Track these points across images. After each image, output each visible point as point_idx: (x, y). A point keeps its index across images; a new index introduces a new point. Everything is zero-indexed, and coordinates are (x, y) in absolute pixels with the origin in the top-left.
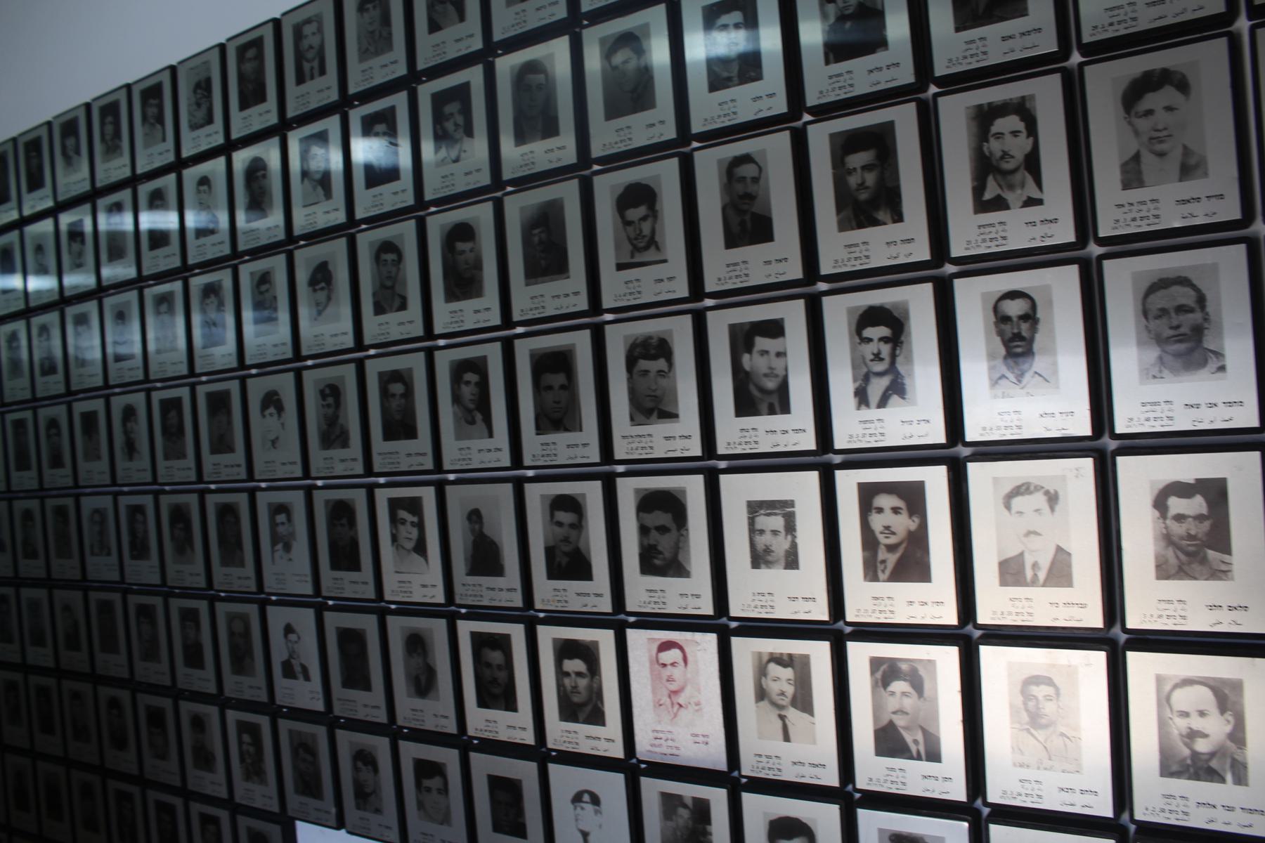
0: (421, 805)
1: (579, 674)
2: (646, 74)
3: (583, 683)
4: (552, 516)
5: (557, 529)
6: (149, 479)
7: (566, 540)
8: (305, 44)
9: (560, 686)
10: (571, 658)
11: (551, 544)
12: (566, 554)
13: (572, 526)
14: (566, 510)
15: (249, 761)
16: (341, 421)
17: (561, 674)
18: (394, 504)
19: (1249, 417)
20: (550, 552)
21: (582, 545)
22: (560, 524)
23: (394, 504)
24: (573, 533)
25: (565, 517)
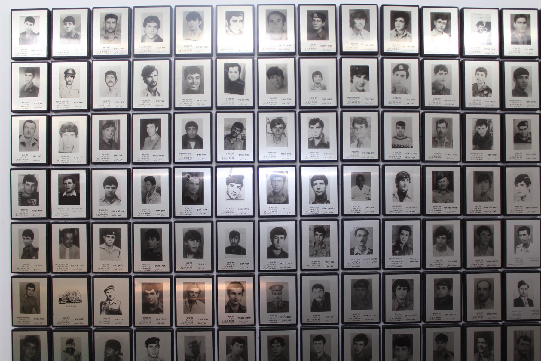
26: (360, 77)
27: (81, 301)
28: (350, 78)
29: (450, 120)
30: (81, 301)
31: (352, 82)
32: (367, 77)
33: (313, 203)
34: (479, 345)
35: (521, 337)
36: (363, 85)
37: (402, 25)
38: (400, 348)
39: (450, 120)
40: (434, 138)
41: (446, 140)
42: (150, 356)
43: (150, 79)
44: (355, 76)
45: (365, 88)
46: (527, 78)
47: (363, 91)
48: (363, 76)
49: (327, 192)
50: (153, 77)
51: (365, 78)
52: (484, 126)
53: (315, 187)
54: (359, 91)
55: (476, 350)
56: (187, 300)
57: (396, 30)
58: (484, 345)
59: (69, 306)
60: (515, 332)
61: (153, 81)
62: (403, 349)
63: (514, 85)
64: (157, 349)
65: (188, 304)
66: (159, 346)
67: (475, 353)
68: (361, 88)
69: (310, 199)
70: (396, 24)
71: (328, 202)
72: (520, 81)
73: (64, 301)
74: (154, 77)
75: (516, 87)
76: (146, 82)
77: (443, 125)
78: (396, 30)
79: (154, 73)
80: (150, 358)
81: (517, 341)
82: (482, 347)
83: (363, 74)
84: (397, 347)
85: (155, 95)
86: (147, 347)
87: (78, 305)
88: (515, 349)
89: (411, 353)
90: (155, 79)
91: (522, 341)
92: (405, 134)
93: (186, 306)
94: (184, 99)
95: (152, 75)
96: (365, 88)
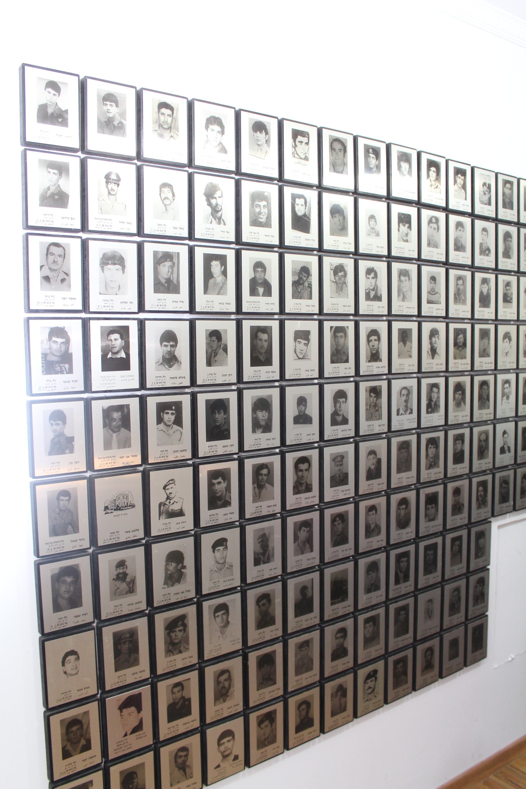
27: (133, 506)
30: (133, 506)
33: (369, 361)
53: (371, 344)
56: (256, 485)
59: (118, 516)
65: (257, 490)
69: (367, 358)
71: (381, 361)
73: (112, 509)
87: (130, 511)
94: (251, 233)
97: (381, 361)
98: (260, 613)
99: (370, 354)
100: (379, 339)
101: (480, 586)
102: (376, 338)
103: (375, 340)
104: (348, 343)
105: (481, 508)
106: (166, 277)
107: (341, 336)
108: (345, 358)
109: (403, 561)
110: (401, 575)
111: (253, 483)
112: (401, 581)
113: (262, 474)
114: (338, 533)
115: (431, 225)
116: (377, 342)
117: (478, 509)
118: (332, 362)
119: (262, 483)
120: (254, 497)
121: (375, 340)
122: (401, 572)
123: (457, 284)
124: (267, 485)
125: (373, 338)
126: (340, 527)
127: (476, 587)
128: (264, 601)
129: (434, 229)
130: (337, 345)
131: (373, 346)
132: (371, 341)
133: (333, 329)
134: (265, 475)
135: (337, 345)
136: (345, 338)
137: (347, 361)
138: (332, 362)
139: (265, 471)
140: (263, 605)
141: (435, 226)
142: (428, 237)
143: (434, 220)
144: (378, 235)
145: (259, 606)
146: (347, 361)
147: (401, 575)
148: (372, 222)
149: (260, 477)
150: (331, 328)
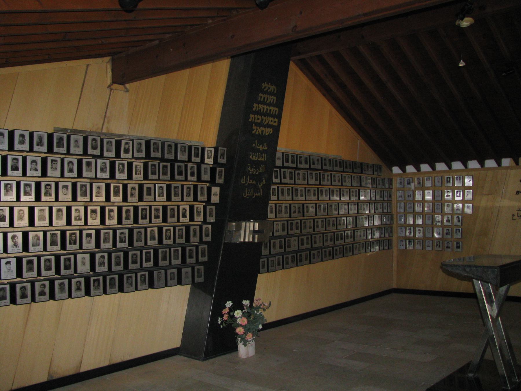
0: (308, 195)
1: (154, 168)
2: (411, 207)
3: (154, 170)
4: (13, 161)
5: (14, 163)
6: (293, 183)
7: (15, 165)
8: (137, 169)
9: (151, 170)
10: (153, 166)
11: (12, 165)
12: (15, 167)
13: (16, 162)
14: (15, 160)
15: (120, 170)
16: (141, 148)
17: (151, 168)
18: (310, 173)
19: (209, 180)
20: (12, 167)
21: (18, 165)
22: (14, 162)
23: (310, 173)
24: (16, 164)
25: (15, 161)
26: (89, 238)
28: (85, 238)
29: (109, 232)
31: (86, 240)
32: (91, 238)
33: (69, 172)
34: (120, 167)
35: (117, 257)
36: (90, 241)
37: (97, 284)
38: (93, 214)
39: (109, 232)
40: (104, 240)
41: (108, 241)
42: (7, 269)
43: (15, 240)
44: (87, 238)
45: (90, 242)
46: (130, 213)
47: (90, 243)
48: (90, 237)
49: (73, 168)
50: (16, 239)
51: (90, 238)
52: (127, 145)
53: (69, 166)
54: (89, 243)
55: (119, 170)
56: (5, 190)
57: (95, 287)
58: (122, 168)
60: (115, 255)
61: (16, 241)
62: (94, 214)
63: (126, 215)
64: (10, 266)
65: (6, 192)
66: (11, 264)
67: (119, 171)
68: (89, 242)
69: (67, 171)
70: (95, 284)
71: (74, 172)
72: (127, 214)
74: (16, 240)
75: (126, 216)
76: (13, 241)
77: (107, 235)
78: (95, 287)
79: (16, 238)
80: (8, 270)
81: (116, 258)
82: (121, 169)
83: (90, 236)
84: (92, 214)
85: (17, 247)
86: (6, 265)
88: (115, 261)
89: (97, 216)
90: (17, 240)
91: (117, 258)
92: (100, 192)
93: (5, 193)
95: (15, 239)
96: (90, 242)
97: (74, 172)
98: (22, 293)
99: (69, 169)
100: (73, 165)
101: (102, 259)
102: (72, 164)
103: (71, 165)
104: (57, 239)
105: (121, 174)
106: (2, 295)
107: (55, 237)
108: (56, 244)
109: (73, 236)
110: (72, 242)
111: (4, 189)
112: (73, 244)
113: (8, 187)
114: (47, 266)
115: (108, 144)
116: (72, 166)
117: (120, 174)
118: (51, 245)
119: (8, 190)
120: (5, 194)
121: (71, 165)
122: (72, 240)
123: (105, 236)
124: (10, 191)
125: (70, 164)
126: (48, 264)
127: (100, 259)
128: (24, 289)
129: (110, 145)
130: (53, 240)
131: (70, 167)
132: (70, 165)
133: (51, 234)
134: (9, 187)
135: (53, 240)
136: (56, 237)
137: (57, 245)
138: (51, 245)
139: (9, 186)
140: (23, 290)
141: (110, 144)
142: (107, 148)
143: (109, 142)
144: (79, 147)
145: (21, 291)
146: (57, 245)
147: (72, 242)
148: (76, 143)
149: (7, 188)
150: (50, 234)
